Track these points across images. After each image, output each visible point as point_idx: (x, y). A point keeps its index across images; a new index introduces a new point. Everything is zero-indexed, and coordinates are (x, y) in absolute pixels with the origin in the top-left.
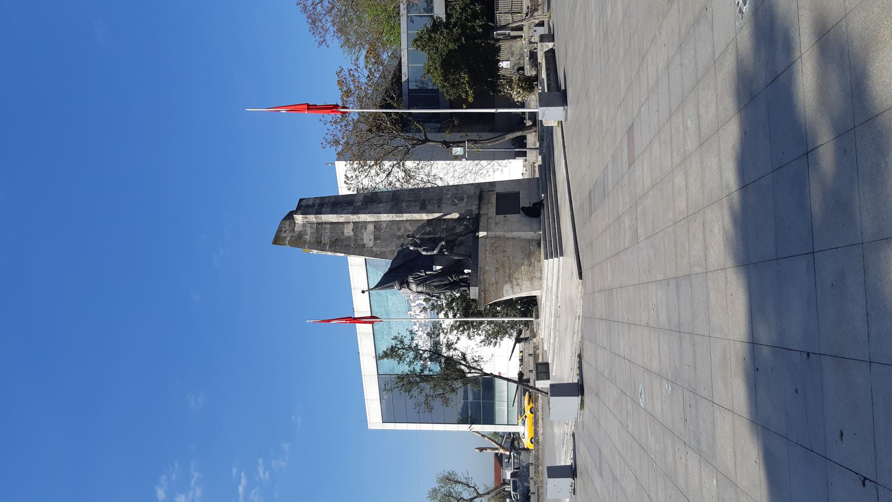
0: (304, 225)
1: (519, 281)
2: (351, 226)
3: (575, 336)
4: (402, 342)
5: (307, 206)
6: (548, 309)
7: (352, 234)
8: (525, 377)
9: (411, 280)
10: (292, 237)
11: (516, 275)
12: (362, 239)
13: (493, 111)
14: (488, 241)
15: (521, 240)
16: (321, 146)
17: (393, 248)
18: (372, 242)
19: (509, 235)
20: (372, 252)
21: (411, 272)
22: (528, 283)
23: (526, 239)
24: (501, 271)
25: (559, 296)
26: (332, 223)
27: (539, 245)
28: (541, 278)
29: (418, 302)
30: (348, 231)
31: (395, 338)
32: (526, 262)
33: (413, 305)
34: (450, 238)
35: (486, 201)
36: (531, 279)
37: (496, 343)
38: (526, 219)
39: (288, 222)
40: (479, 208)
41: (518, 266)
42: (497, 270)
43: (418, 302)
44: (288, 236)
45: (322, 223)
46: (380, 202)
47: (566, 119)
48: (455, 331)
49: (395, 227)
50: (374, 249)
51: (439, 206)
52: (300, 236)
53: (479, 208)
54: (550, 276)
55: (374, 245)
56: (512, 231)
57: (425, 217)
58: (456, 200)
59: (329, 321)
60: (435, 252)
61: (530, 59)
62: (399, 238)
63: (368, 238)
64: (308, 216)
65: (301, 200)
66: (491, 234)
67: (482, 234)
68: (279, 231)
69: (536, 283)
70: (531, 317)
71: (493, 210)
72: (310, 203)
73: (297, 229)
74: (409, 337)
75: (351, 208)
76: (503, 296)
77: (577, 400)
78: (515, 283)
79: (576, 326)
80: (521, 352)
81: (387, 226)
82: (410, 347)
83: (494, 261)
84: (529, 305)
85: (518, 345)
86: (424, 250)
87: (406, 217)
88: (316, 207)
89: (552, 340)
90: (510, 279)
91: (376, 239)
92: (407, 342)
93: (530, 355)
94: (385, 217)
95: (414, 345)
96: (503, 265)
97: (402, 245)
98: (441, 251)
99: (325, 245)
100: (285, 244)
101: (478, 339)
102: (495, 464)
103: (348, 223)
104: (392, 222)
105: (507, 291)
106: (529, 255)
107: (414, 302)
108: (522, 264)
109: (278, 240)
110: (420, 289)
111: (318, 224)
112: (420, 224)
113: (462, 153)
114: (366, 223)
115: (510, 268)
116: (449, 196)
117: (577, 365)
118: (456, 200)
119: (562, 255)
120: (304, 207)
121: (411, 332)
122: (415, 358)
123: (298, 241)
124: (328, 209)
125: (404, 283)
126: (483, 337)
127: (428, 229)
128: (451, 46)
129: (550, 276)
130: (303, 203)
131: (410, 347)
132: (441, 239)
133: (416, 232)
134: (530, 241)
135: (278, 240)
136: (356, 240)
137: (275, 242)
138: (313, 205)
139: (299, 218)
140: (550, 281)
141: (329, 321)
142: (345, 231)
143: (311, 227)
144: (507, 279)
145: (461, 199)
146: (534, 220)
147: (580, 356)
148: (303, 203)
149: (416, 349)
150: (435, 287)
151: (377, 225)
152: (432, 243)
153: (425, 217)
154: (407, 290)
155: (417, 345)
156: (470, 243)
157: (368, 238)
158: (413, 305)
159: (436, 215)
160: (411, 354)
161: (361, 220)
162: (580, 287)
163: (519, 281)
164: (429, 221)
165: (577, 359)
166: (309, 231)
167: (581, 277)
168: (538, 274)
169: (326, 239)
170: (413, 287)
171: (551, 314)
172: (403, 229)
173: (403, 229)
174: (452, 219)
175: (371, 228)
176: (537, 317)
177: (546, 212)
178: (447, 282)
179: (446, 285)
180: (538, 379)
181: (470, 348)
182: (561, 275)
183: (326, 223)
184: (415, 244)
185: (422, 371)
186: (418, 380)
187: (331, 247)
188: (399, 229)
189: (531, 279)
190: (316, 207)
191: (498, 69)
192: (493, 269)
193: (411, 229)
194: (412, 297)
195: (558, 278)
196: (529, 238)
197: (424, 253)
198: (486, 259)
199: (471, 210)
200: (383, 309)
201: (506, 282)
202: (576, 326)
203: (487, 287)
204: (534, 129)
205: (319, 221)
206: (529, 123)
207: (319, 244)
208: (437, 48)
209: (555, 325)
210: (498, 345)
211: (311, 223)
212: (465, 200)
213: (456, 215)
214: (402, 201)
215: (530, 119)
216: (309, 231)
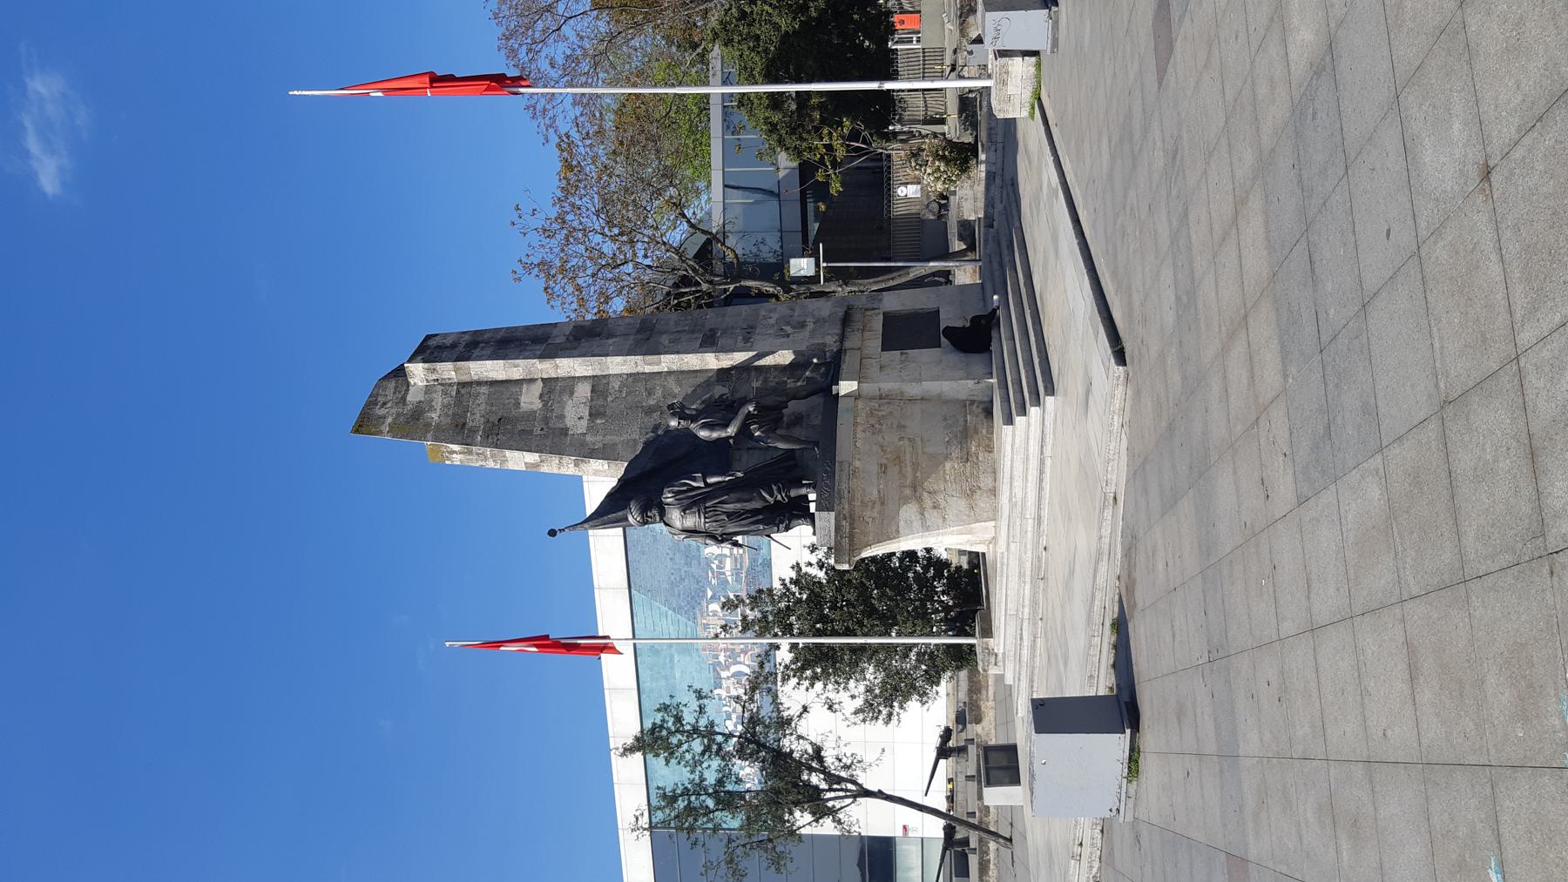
0: (428, 389)
1: (940, 498)
2: (538, 388)
3: (1103, 567)
4: (678, 719)
5: (440, 348)
6: (1014, 564)
7: (538, 405)
8: (958, 836)
9: (668, 497)
10: (398, 415)
12: (562, 417)
13: (873, 86)
14: (860, 404)
15: (941, 400)
16: (512, 276)
17: (634, 436)
18: (584, 423)
19: (913, 390)
20: (583, 444)
21: (669, 482)
22: (962, 504)
23: (957, 401)
24: (893, 471)
25: (1045, 514)
26: (493, 383)
27: (989, 413)
28: (994, 492)
29: (734, 669)
30: (530, 400)
31: (664, 708)
32: (956, 453)
33: (724, 674)
34: (770, 401)
35: (859, 325)
36: (970, 494)
37: (890, 715)
38: (955, 358)
39: (392, 384)
40: (842, 338)
41: (937, 461)
42: (884, 468)
43: (734, 669)
44: (389, 414)
45: (470, 384)
46: (610, 335)
47: (1055, 43)
48: (794, 681)
49: (640, 387)
50: (589, 438)
51: (746, 340)
52: (418, 413)
53: (842, 338)
54: (1019, 466)
55: (589, 429)
56: (920, 381)
57: (712, 361)
58: (788, 329)
59: (497, 644)
60: (731, 430)
61: (961, 112)
62: (649, 411)
63: (575, 414)
64: (439, 366)
65: (428, 337)
66: (869, 388)
67: (846, 387)
68: (372, 403)
69: (983, 502)
70: (973, 635)
71: (874, 343)
72: (448, 341)
73: (412, 397)
74: (694, 705)
75: (540, 348)
76: (894, 535)
77: (1117, 744)
78: (928, 502)
79: (1101, 581)
80: (950, 781)
81: (623, 385)
82: (695, 730)
83: (876, 448)
84: (962, 592)
85: (942, 762)
86: (704, 426)
87: (668, 362)
88: (461, 348)
89: (1025, 652)
90: (915, 491)
91: (593, 415)
92: (689, 718)
93: (969, 778)
94: (618, 365)
95: (703, 723)
96: (898, 460)
97: (656, 428)
98: (744, 431)
99: (473, 431)
100: (381, 433)
101: (850, 706)
102: (497, 330)
103: (532, 380)
104: (635, 377)
105: (909, 523)
106: (965, 435)
107: (727, 668)
108: (947, 457)
109: (365, 423)
110: (691, 521)
111: (463, 384)
112: (700, 380)
113: (811, 273)
114: (571, 382)
115: (915, 466)
116: (772, 321)
117: (1108, 657)
118: (788, 329)
119: (1051, 390)
120: (429, 351)
121: (700, 695)
122: (707, 749)
123: (413, 423)
124: (488, 351)
125: (652, 508)
126: (859, 702)
127: (719, 391)
128: (785, 23)
129: (1019, 466)
130: (432, 343)
131: (695, 730)
132: (745, 401)
133: (690, 397)
134: (965, 404)
135: (365, 423)
136: (546, 420)
137: (357, 431)
138: (454, 345)
139: (418, 373)
140: (1018, 484)
141: (497, 644)
142: (523, 399)
143: (445, 393)
144: (908, 492)
145: (802, 325)
146: (976, 360)
147: (1120, 626)
148: (432, 343)
149: (710, 732)
150: (729, 515)
151: (599, 384)
152: (720, 411)
153: (712, 361)
154: (659, 527)
155: (712, 724)
156: (817, 420)
157: (575, 414)
158: (724, 674)
159: (739, 357)
160: (697, 745)
161: (562, 373)
162: (1119, 392)
164: (723, 374)
165: (1109, 638)
166: (438, 400)
167: (1120, 356)
168: (985, 481)
169: (476, 418)
170: (675, 515)
171: (1021, 575)
172: (659, 393)
173: (659, 393)
174: (776, 367)
175: (583, 391)
176: (987, 632)
177: (1007, 342)
178: (757, 505)
179: (755, 512)
180: (989, 784)
181: (832, 738)
182: (1048, 451)
183: (479, 383)
184: (680, 412)
185: (720, 782)
186: (710, 803)
187: (486, 436)
188: (650, 393)
189: (970, 494)
190: (461, 348)
192: (875, 469)
193: (679, 392)
194: (722, 659)
195: (1042, 462)
196: (963, 396)
197: (703, 434)
198: (857, 446)
199: (824, 345)
200: (663, 683)
202: (1106, 532)
203: (858, 511)
204: (971, 256)
205: (465, 378)
206: (957, 246)
207: (459, 431)
208: (757, 38)
209: (1034, 603)
210: (895, 718)
211: (446, 385)
212: (810, 326)
213: (784, 357)
214: (662, 333)
215: (961, 238)
216: (438, 400)
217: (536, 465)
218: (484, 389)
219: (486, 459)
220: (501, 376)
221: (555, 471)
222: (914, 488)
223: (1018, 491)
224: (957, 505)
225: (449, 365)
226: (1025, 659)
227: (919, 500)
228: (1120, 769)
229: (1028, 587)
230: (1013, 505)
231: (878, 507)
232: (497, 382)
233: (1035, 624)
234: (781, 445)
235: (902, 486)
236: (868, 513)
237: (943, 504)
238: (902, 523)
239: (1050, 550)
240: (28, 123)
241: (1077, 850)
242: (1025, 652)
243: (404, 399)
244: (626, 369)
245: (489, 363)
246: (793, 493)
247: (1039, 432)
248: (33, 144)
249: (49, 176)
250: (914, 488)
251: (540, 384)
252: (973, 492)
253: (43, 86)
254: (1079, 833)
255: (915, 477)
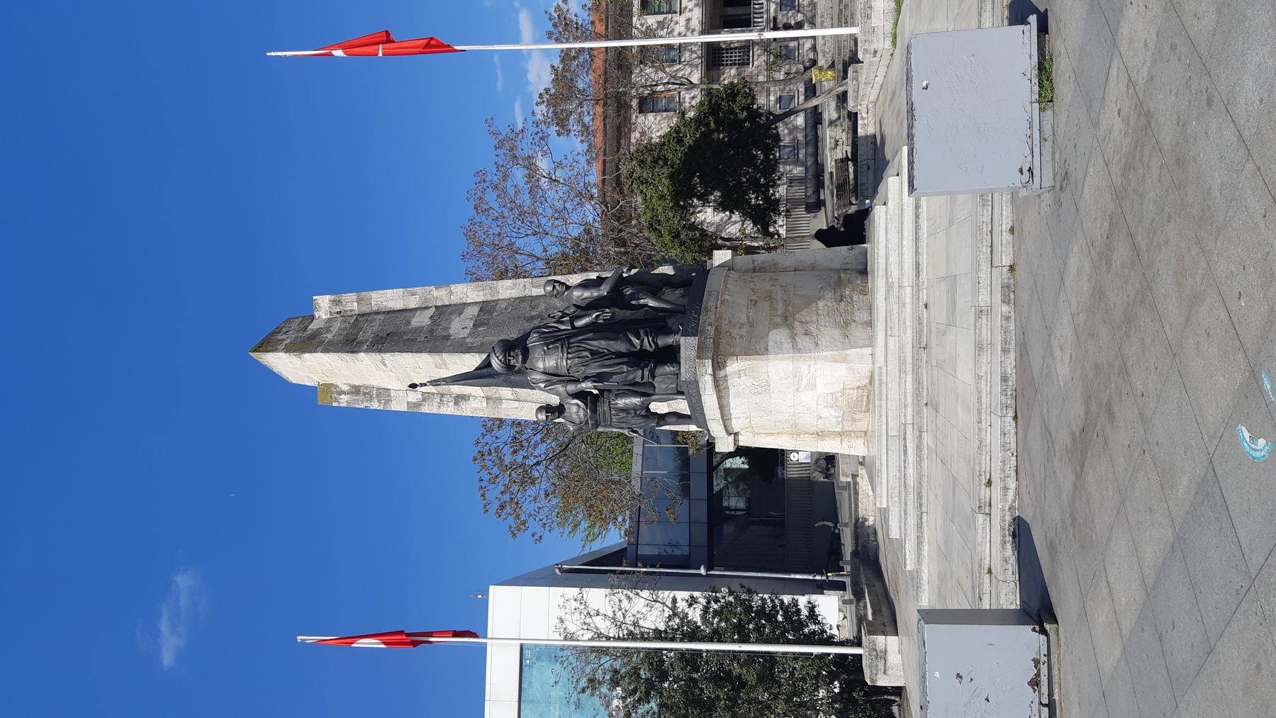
11: (804, 315)
25: (924, 259)
28: (870, 324)
49: (526, 305)
69: (858, 332)
78: (799, 328)
89: (911, 471)
106: (839, 284)
115: (787, 303)
144: (778, 320)
161: (455, 299)
163: (813, 328)
168: (862, 316)
171: (902, 362)
178: (621, 347)
179: (619, 355)
183: (377, 313)
191: (749, 501)
195: (917, 228)
196: (836, 265)
201: (776, 326)
205: (366, 309)
217: (418, 405)
218: (381, 317)
219: (371, 399)
220: (398, 305)
221: (435, 411)
222: (786, 318)
223: (894, 269)
224: (830, 334)
225: (353, 296)
226: (911, 482)
227: (791, 328)
228: (1026, 88)
229: (909, 378)
230: (889, 287)
231: (745, 328)
232: (394, 311)
233: (919, 412)
234: (652, 303)
235: (772, 315)
236: (735, 332)
237: (815, 331)
238: (771, 344)
239: (931, 306)
240: (165, 611)
241: (985, 493)
242: (911, 471)
243: (306, 328)
244: (515, 293)
245: (389, 292)
246: (661, 342)
247: (920, 244)
248: (164, 626)
249: (167, 659)
250: (786, 318)
251: (433, 309)
252: (847, 324)
253: (183, 581)
254: (985, 465)
255: (787, 311)
